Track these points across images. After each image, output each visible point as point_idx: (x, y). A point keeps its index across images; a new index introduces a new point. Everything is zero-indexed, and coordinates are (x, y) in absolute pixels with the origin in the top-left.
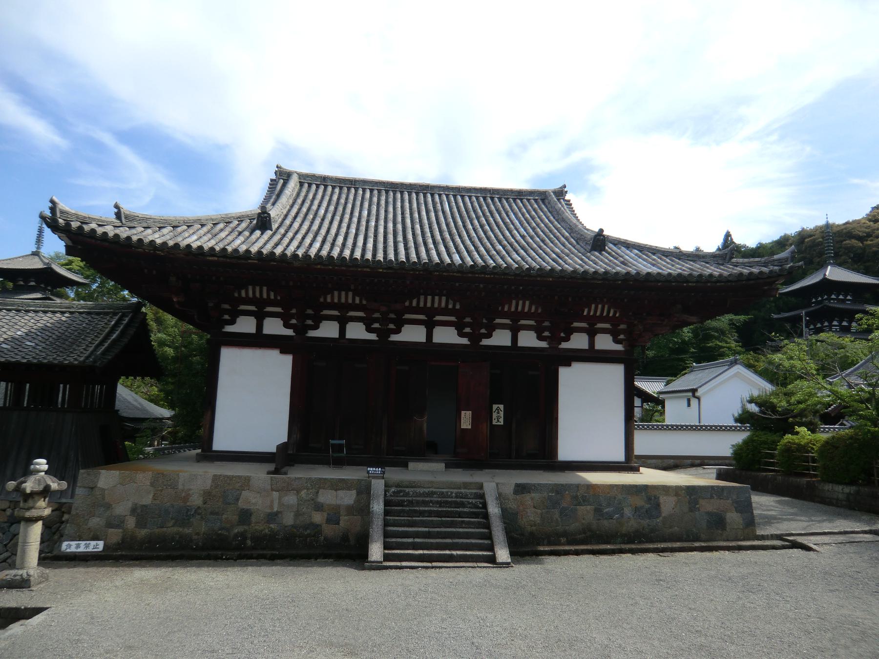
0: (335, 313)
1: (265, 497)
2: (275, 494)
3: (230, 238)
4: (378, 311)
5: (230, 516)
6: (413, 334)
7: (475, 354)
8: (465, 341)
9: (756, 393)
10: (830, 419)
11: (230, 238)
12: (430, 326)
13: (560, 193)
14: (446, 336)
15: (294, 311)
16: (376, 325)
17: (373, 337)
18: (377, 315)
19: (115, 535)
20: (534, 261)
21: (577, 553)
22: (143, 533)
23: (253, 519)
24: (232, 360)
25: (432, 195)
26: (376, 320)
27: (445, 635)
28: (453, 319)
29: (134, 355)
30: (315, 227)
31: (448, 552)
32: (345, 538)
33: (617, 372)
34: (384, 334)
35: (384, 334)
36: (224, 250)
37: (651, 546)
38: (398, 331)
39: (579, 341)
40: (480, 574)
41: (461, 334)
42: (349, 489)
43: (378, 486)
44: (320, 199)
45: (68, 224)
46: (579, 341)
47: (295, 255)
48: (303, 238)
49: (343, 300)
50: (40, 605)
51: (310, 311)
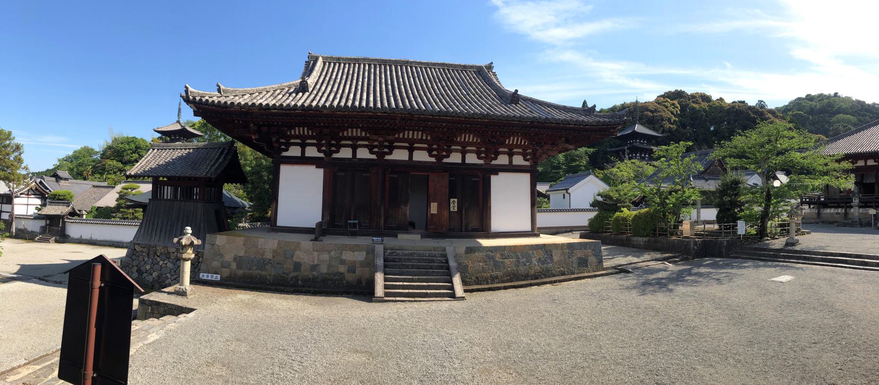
0: (350, 142)
1: (309, 255)
2: (316, 254)
3: (285, 98)
4: (377, 141)
5: (289, 266)
6: (400, 155)
8: (433, 160)
9: (601, 191)
10: (636, 204)
11: (285, 98)
12: (411, 150)
13: (490, 67)
14: (421, 156)
15: (324, 142)
16: (376, 150)
17: (374, 157)
19: (226, 272)
21: (505, 288)
22: (240, 272)
23: (302, 268)
25: (411, 67)
26: (376, 147)
27: (427, 346)
28: (426, 146)
29: (233, 171)
30: (335, 89)
31: (424, 291)
32: (359, 281)
33: (526, 178)
34: (381, 155)
35: (381, 155)
36: (281, 105)
38: (390, 153)
39: (503, 160)
40: (446, 305)
41: (431, 156)
42: (361, 250)
43: (380, 249)
44: (339, 73)
45: (194, 98)
46: (503, 160)
47: (324, 106)
48: (328, 96)
49: (355, 134)
50: (192, 307)
51: (333, 142)
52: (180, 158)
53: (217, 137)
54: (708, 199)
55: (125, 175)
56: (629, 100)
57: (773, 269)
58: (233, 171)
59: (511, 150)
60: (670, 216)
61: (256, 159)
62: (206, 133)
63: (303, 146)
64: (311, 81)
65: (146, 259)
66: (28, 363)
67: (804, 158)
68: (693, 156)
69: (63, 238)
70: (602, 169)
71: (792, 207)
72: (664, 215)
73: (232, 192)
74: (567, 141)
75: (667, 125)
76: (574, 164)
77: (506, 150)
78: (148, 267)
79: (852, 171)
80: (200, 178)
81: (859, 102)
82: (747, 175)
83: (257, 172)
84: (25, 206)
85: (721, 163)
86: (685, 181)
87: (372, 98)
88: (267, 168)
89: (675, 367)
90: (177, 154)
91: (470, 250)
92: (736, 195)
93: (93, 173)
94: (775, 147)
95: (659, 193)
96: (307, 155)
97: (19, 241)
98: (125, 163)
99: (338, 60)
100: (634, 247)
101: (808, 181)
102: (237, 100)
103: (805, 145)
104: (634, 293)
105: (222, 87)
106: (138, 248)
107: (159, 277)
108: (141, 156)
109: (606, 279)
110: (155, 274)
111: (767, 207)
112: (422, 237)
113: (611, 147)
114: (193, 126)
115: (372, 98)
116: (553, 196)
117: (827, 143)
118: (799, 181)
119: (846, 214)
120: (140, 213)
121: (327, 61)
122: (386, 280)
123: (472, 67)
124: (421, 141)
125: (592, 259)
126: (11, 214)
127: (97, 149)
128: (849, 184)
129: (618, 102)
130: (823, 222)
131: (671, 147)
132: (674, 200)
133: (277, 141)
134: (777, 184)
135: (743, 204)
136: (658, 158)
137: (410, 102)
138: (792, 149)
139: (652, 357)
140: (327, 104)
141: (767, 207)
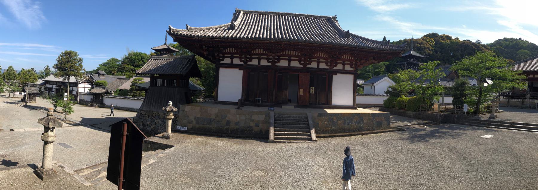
1: (235, 117)
6: (284, 63)
7: (305, 70)
10: (410, 93)
12: (290, 61)
13: (335, 18)
14: (295, 64)
16: (271, 60)
17: (270, 64)
18: (271, 57)
19: (190, 126)
20: (326, 39)
21: (338, 136)
22: (198, 126)
24: (223, 72)
29: (195, 72)
30: (249, 28)
32: (261, 131)
33: (351, 77)
34: (273, 63)
35: (273, 63)
36: (220, 36)
37: (360, 133)
38: (278, 62)
39: (339, 67)
40: (306, 145)
41: (300, 64)
43: (272, 114)
44: (250, 19)
45: (174, 33)
46: (339, 67)
47: (243, 37)
51: (248, 56)
52: (167, 64)
53: (187, 52)
54: (448, 92)
55: (136, 73)
56: (408, 37)
57: (482, 131)
58: (195, 72)
59: (344, 62)
60: (427, 101)
61: (207, 64)
62: (180, 50)
63: (232, 58)
64: (237, 23)
65: (147, 118)
66: (88, 168)
67: (501, 72)
68: (441, 69)
69: (102, 105)
70: (392, 73)
71: (494, 98)
72: (424, 100)
73: (194, 82)
74: (374, 59)
75: (428, 52)
76: (377, 70)
77: (341, 62)
78: (148, 123)
79: (526, 80)
80: (177, 75)
81: (532, 44)
82: (470, 79)
83: (207, 71)
84: (84, 88)
85: (456, 72)
86: (437, 82)
87: (269, 33)
88: (213, 69)
89: (427, 183)
90: (164, 62)
91: (320, 115)
92: (464, 90)
93: (117, 72)
94: (486, 65)
95: (422, 88)
96: (291, 65)
97: (81, 105)
98: (135, 66)
99: (252, 13)
100: (407, 116)
101: (504, 84)
102: (197, 34)
103: (502, 65)
104: (407, 143)
105: (189, 27)
106: (143, 112)
107: (154, 128)
108: (144, 63)
109: (392, 134)
110: (152, 127)
111: (480, 97)
112: (295, 107)
113: (398, 62)
114: (173, 46)
115: (269, 33)
116: (366, 88)
117: (514, 64)
118: (499, 83)
119: (523, 102)
120: (143, 94)
121: (246, 13)
122: (275, 131)
123: (325, 17)
124: (295, 56)
125: (385, 123)
126: (77, 91)
127: (120, 59)
128: (525, 86)
129: (403, 38)
130: (511, 106)
131: (429, 64)
132: (430, 92)
133: (218, 55)
134: (486, 85)
135: (467, 95)
136: (422, 69)
137: (289, 35)
138: (494, 67)
139: (414, 177)
140: (245, 36)
141: (480, 97)
